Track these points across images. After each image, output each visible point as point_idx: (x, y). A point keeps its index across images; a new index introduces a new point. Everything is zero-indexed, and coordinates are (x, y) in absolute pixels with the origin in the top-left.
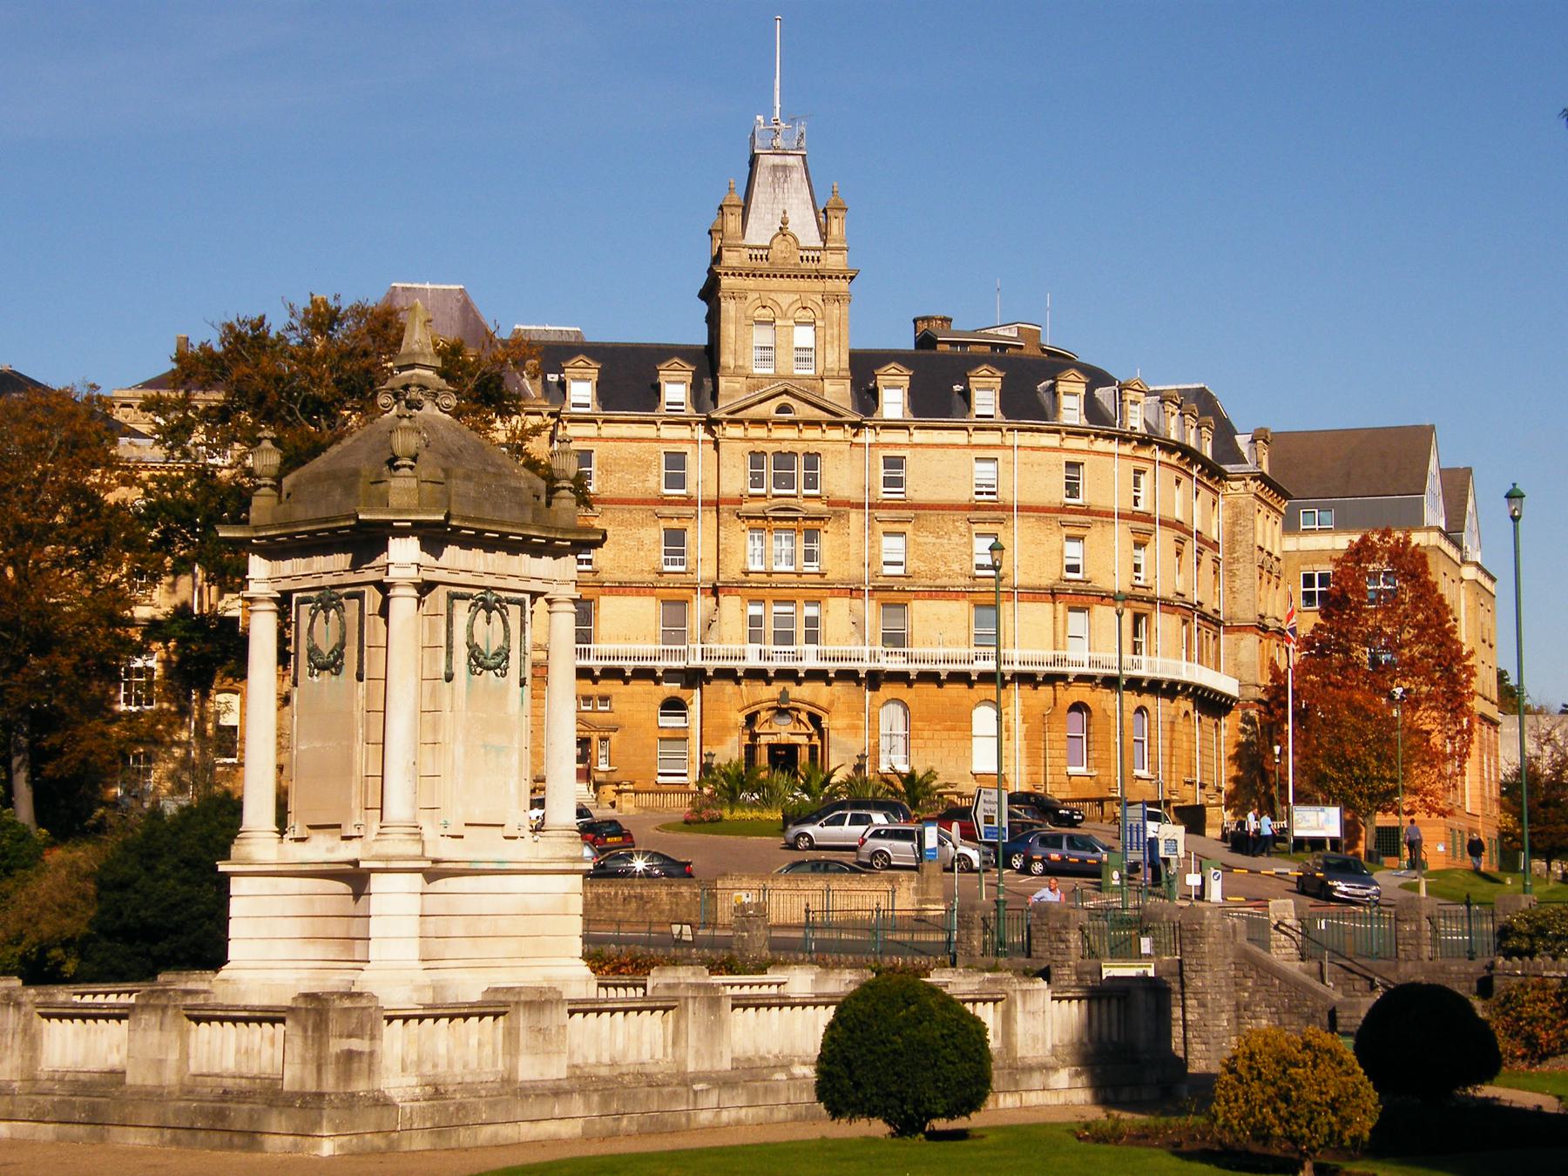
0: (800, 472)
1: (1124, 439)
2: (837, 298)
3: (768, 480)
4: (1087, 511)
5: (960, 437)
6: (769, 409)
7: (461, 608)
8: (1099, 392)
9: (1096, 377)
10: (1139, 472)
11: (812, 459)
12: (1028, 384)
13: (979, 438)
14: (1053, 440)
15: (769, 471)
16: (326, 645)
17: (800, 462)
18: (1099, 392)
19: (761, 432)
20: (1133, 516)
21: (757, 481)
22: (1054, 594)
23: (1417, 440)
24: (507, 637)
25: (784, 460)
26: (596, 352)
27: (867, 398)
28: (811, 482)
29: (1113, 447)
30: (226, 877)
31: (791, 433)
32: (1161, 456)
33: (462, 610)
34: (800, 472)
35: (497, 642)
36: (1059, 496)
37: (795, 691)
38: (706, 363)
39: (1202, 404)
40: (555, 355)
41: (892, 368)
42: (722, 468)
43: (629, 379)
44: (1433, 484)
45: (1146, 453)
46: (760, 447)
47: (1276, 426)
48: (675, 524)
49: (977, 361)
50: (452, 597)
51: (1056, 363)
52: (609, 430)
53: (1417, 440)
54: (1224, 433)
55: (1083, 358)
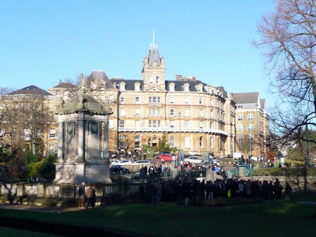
0: (157, 100)
1: (209, 94)
2: (163, 72)
3: (152, 101)
4: (203, 106)
5: (183, 94)
6: (152, 90)
7: (90, 124)
8: (205, 87)
9: (205, 85)
10: (211, 123)
11: (159, 98)
12: (193, 85)
13: (186, 94)
14: (198, 95)
15: (152, 100)
16: (70, 130)
17: (157, 98)
18: (205, 87)
19: (151, 93)
20: (210, 107)
21: (150, 101)
22: (198, 119)
23: (256, 94)
24: (97, 128)
25: (154, 98)
26: (125, 81)
27: (167, 88)
28: (159, 101)
29: (207, 95)
30: (55, 165)
31: (156, 94)
32: (215, 97)
33: (90, 124)
34: (157, 100)
35: (96, 129)
36: (199, 104)
37: (157, 135)
38: (142, 83)
39: (222, 89)
40: (118, 82)
41: (172, 83)
42: (144, 98)
43: (130, 85)
44: (259, 101)
45: (212, 97)
46: (151, 96)
47: (234, 92)
48: (172, 109)
49: (185, 82)
50: (89, 122)
51: (199, 82)
52: (127, 93)
53: (256, 94)
54: (225, 93)
55: (203, 82)
